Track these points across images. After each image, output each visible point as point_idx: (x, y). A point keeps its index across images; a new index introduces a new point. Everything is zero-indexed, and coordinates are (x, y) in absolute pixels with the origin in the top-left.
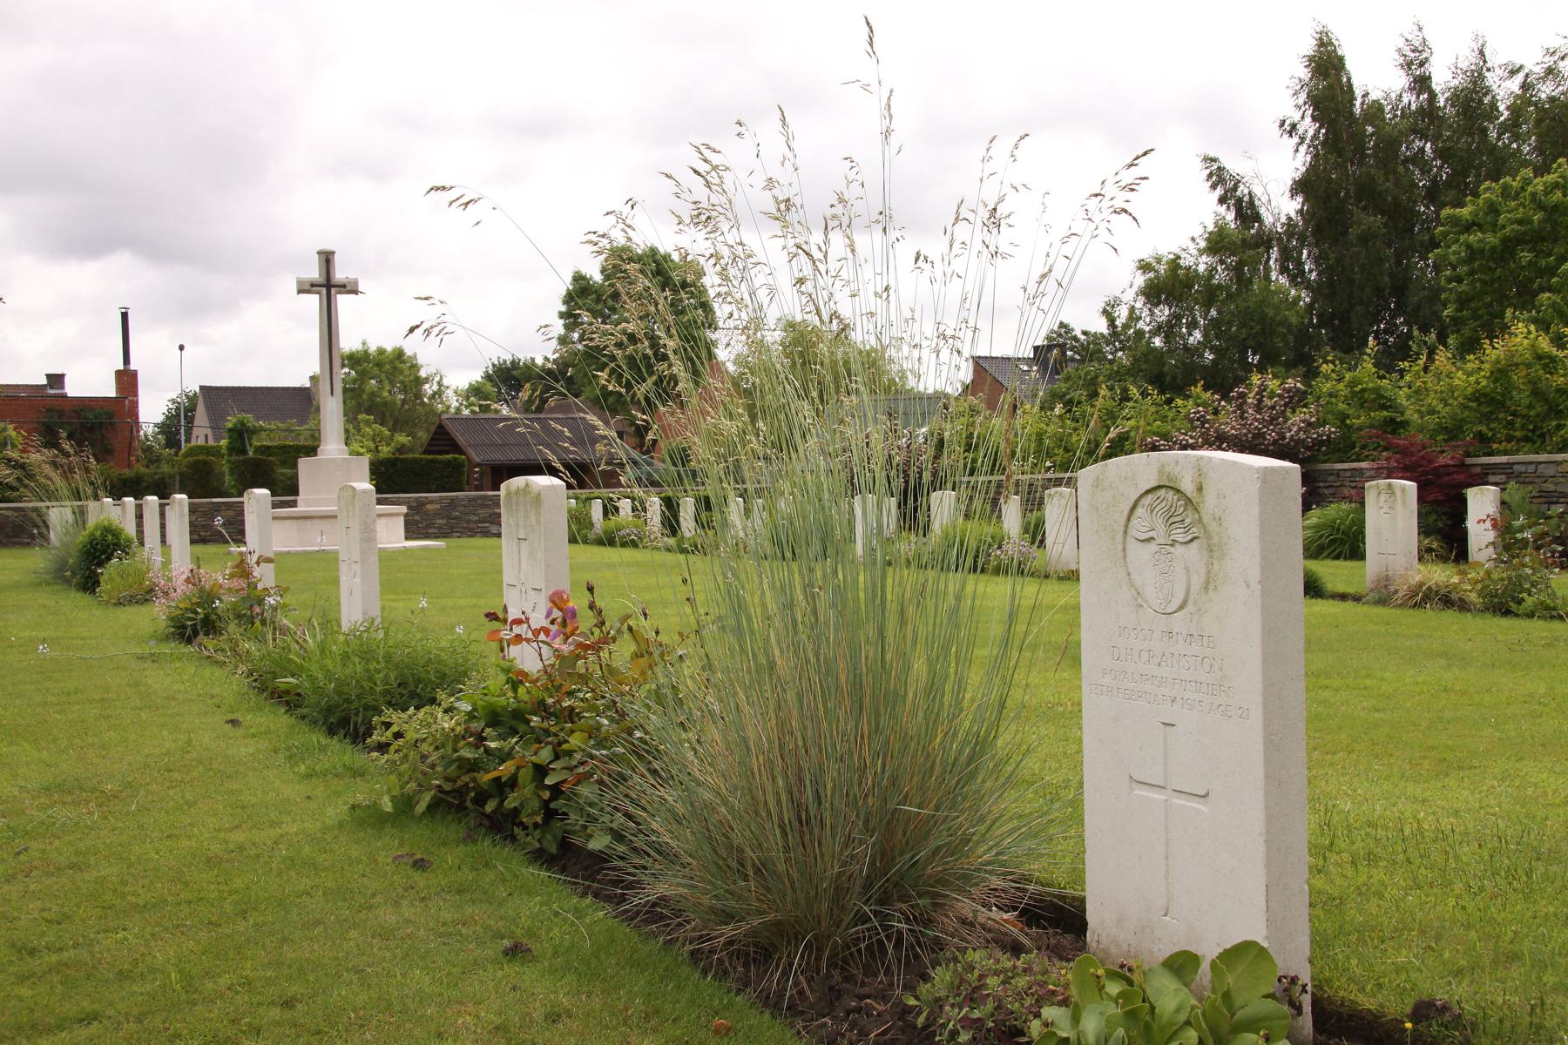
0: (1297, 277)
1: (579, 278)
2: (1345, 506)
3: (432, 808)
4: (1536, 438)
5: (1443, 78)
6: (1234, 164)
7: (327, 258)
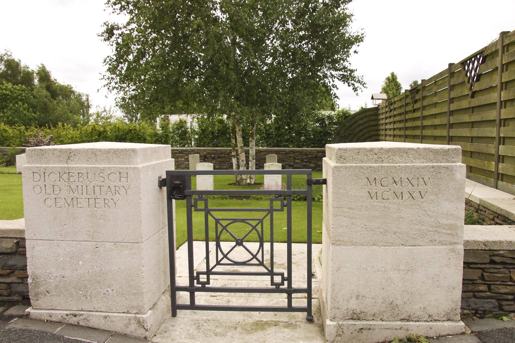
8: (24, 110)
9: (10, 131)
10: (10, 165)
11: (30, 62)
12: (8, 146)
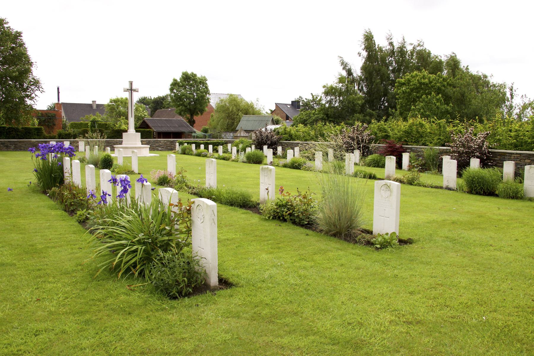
0: (361, 90)
1: (175, 80)
2: (376, 155)
3: (273, 218)
4: (417, 142)
5: (396, 45)
6: (346, 60)
7: (131, 83)
8: (437, 102)
9: (427, 126)
10: (426, 170)
11: (440, 51)
12: (424, 144)
